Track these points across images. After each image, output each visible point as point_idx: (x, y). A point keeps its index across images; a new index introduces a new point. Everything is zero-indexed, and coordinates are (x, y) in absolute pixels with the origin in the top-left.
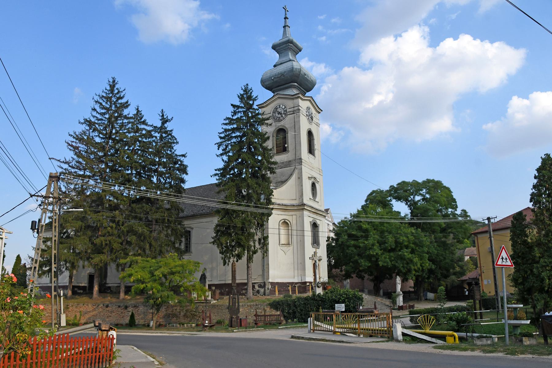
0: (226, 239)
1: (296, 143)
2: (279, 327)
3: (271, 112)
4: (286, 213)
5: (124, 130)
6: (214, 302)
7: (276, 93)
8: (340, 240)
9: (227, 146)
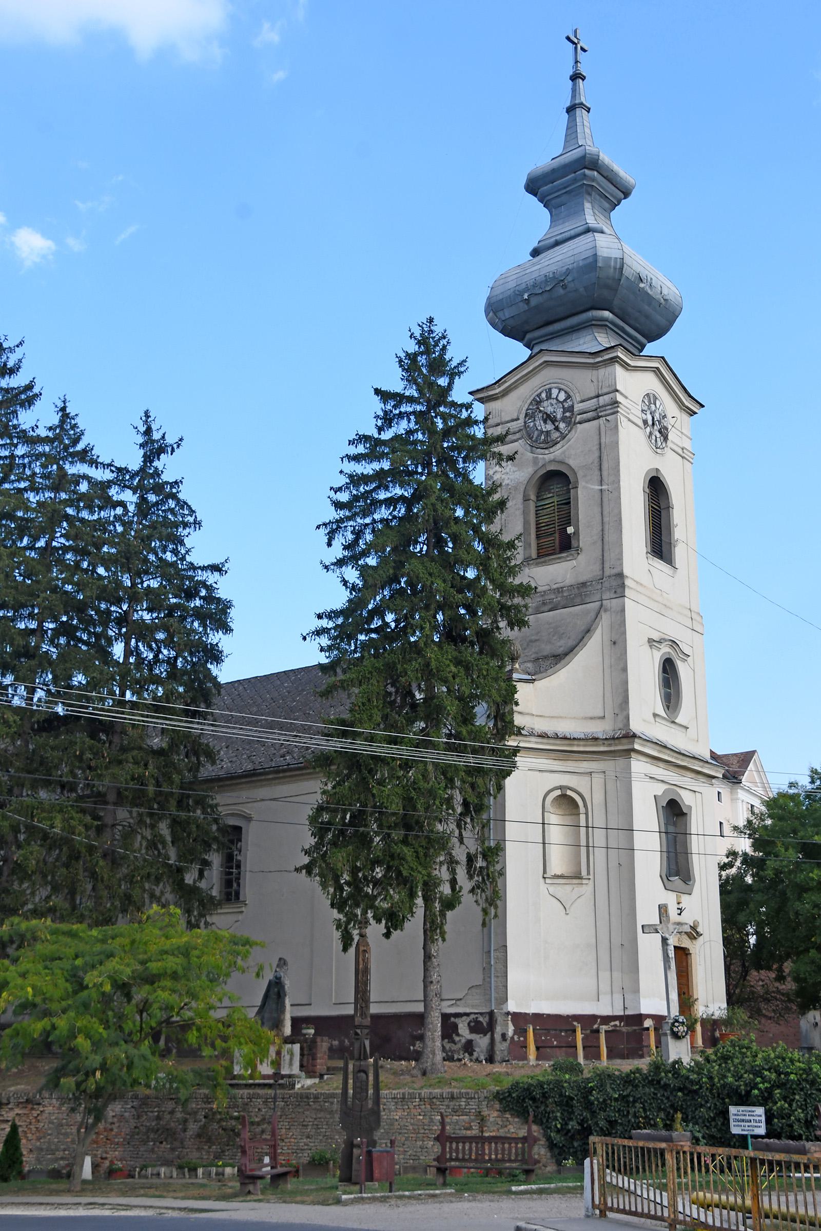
0: (348, 855)
1: (606, 519)
2: (514, 1188)
3: (519, 412)
4: (570, 766)
5: (18, 481)
6: (305, 1083)
7: (536, 349)
8: (771, 863)
9: (358, 534)
